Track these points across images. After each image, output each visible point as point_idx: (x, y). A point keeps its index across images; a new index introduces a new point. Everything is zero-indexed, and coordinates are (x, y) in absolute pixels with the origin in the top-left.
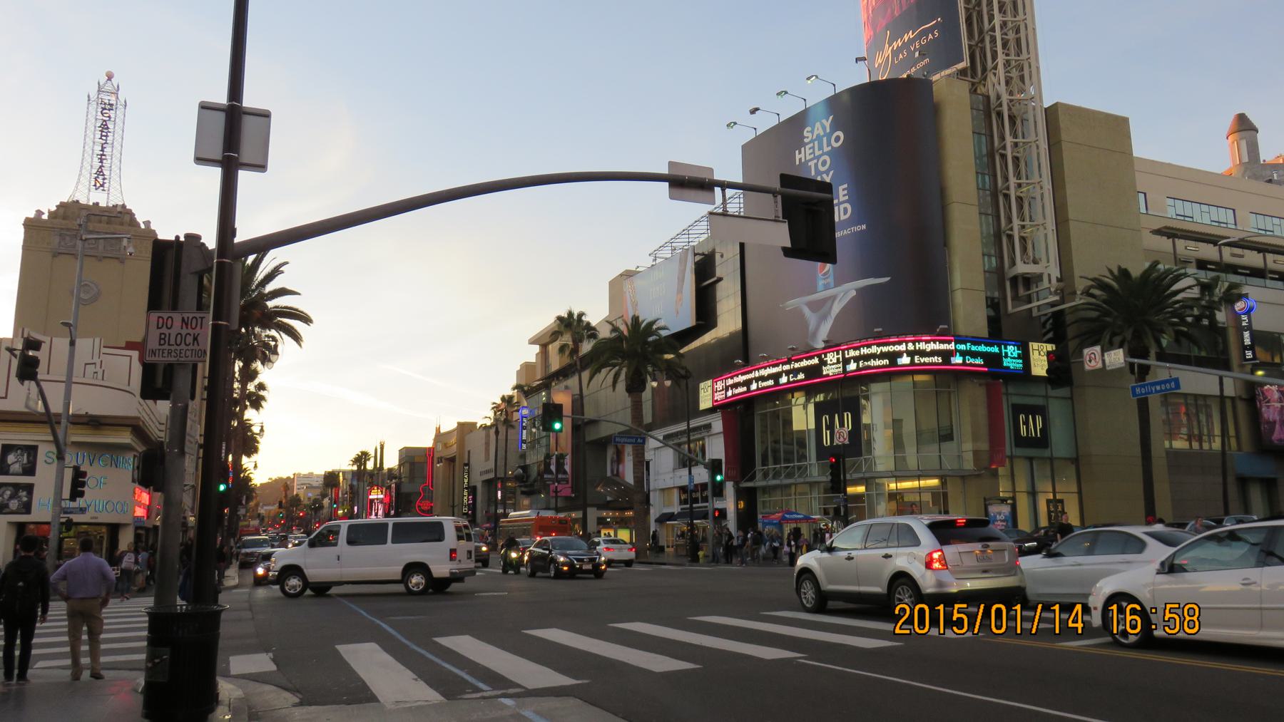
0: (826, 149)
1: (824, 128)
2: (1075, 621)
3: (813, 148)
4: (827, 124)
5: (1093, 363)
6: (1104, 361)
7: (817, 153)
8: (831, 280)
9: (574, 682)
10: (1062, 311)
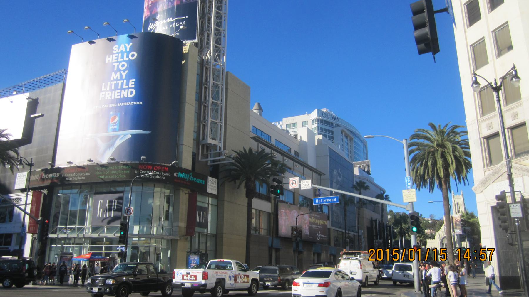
0: (125, 59)
1: (126, 48)
2: (467, 256)
3: (118, 56)
4: (129, 47)
5: (294, 185)
6: (300, 185)
7: (120, 60)
8: (117, 127)
9: (309, 271)
10: (218, 165)
